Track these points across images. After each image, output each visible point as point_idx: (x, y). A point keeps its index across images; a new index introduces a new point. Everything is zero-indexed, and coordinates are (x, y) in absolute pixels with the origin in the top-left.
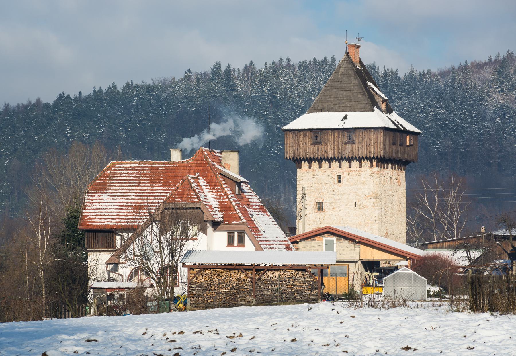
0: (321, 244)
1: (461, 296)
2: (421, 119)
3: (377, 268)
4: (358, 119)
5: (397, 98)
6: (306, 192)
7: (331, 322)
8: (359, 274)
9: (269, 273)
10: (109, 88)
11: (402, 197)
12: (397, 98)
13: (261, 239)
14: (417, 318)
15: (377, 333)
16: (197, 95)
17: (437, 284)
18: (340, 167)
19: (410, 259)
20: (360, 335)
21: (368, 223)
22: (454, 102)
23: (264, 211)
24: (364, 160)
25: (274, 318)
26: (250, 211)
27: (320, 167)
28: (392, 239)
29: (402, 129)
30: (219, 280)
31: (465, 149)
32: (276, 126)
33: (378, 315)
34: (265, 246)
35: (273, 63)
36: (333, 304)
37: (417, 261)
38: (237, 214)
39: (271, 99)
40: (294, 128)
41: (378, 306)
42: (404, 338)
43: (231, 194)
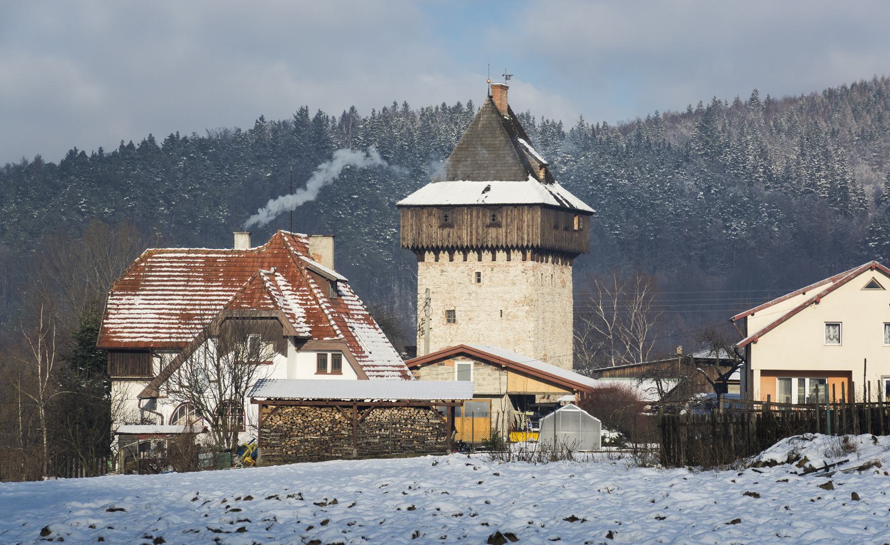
1: (649, 445)
6: (431, 296)
7: (465, 481)
8: (506, 414)
9: (377, 412)
10: (144, 142)
13: (366, 363)
14: (587, 476)
15: (531, 498)
17: (615, 427)
18: (480, 260)
20: (506, 501)
22: (640, 168)
23: (371, 323)
24: (514, 251)
26: (350, 322)
27: (451, 260)
28: (552, 364)
30: (304, 422)
31: (655, 236)
32: (389, 200)
34: (372, 373)
35: (385, 109)
37: (588, 395)
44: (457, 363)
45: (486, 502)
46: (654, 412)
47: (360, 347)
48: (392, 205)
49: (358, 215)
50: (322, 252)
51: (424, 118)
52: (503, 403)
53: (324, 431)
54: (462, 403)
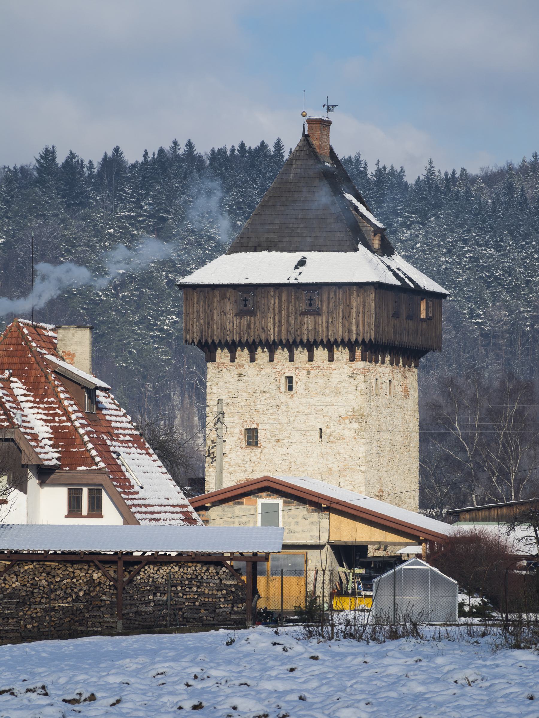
0: (252, 512)
1: (524, 616)
2: (449, 265)
3: (362, 560)
4: (328, 267)
5: (402, 225)
6: (225, 409)
7: (272, 668)
8: (327, 572)
9: (151, 570)
11: (412, 419)
12: (402, 225)
13: (136, 502)
14: (440, 660)
15: (362, 691)
16: (6, 212)
17: (477, 591)
18: (291, 359)
19: (425, 541)
20: (328, 696)
21: (345, 470)
22: (511, 233)
23: (142, 447)
24: (338, 347)
25: (159, 662)
26: (114, 446)
27: (253, 360)
28: (391, 502)
29: (412, 286)
30: (50, 583)
31: (532, 326)
32: (167, 277)
33: (364, 654)
34: (144, 516)
35: (161, 151)
36: (276, 633)
37: (440, 545)
38: (89, 451)
39: (156, 224)
40: (200, 282)
41: (364, 636)
42: (413, 700)
43: (75, 411)
44: (260, 501)
45: (301, 698)
46: (531, 569)
47: (128, 480)
48: (171, 283)
49: (124, 296)
50: (76, 350)
51: (216, 164)
52: (324, 557)
53: (78, 596)
54: (266, 557)
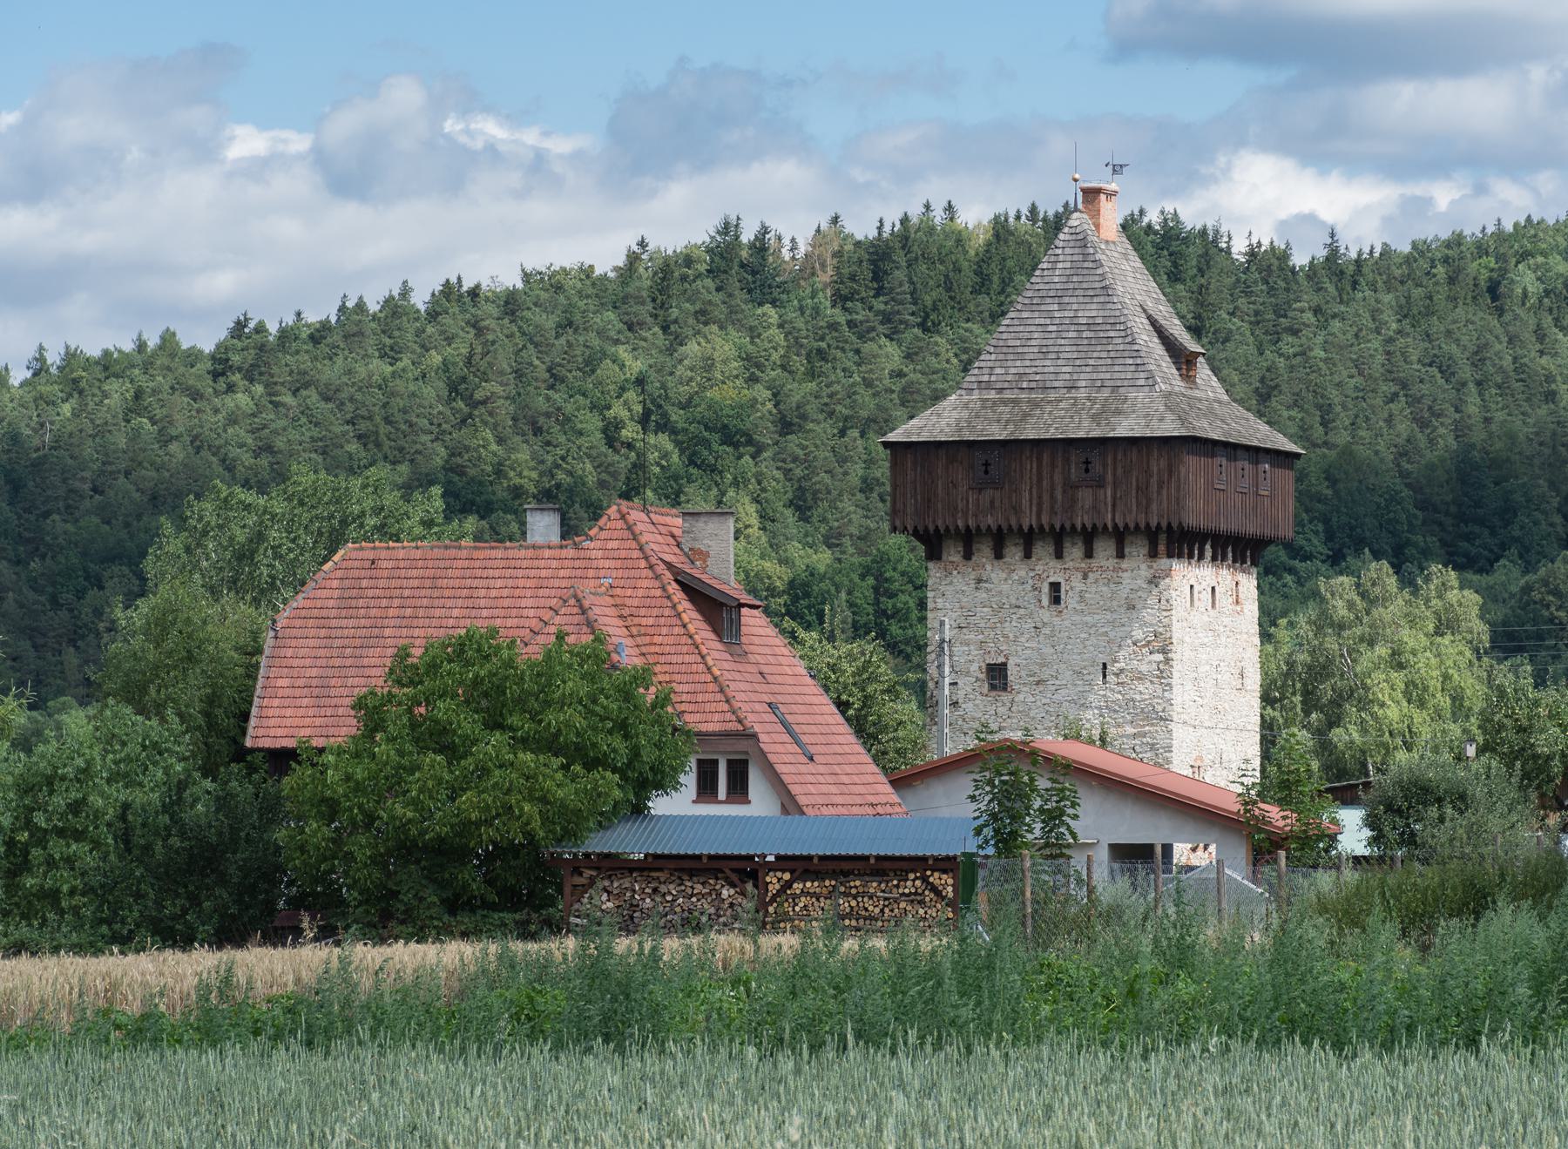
10: (389, 301)
35: (905, 220)
